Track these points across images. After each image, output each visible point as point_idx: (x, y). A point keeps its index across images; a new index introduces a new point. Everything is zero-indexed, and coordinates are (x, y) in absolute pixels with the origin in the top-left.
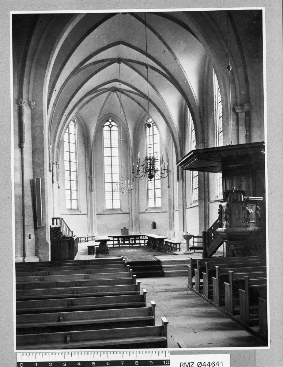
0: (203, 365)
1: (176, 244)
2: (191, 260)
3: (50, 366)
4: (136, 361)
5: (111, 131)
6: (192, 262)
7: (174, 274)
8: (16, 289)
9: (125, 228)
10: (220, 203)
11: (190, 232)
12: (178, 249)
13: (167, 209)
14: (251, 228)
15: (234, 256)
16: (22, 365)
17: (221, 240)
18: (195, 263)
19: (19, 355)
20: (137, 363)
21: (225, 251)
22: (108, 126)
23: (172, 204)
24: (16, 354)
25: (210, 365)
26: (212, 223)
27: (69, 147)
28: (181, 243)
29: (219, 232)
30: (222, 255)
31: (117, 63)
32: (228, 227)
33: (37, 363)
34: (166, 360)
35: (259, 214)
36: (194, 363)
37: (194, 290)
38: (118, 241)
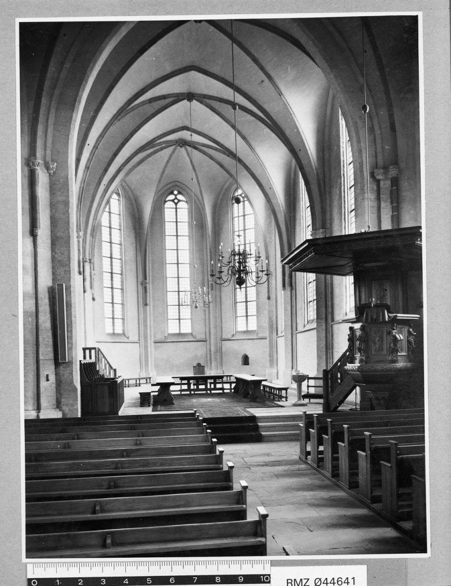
0: (323, 583)
1: (280, 389)
2: (304, 416)
3: (79, 584)
4: (217, 576)
5: (176, 208)
6: (306, 419)
7: (277, 438)
8: (26, 461)
9: (199, 365)
10: (351, 325)
11: (303, 370)
12: (284, 397)
13: (267, 334)
14: (401, 364)
15: (372, 408)
16: (34, 583)
17: (353, 383)
18: (310, 420)
19: (30, 567)
20: (218, 579)
21: (358, 401)
22: (173, 201)
23: (275, 326)
24: (26, 565)
25: (334, 583)
26: (337, 355)
27: (110, 235)
28: (288, 388)
29: (349, 371)
30: (354, 407)
31: (186, 100)
32: (364, 363)
33: (59, 579)
34: (264, 575)
35: (413, 342)
36: (308, 579)
37: (310, 462)
38: (189, 384)
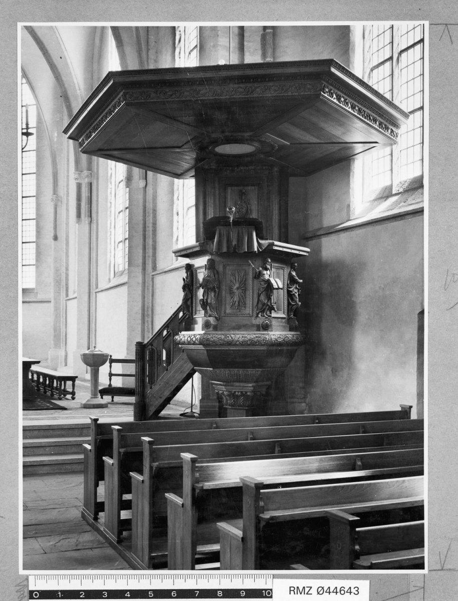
2: (93, 427)
6: (97, 434)
7: (46, 468)
10: (187, 261)
11: (102, 347)
12: (69, 393)
13: (51, 295)
14: (277, 333)
15: (222, 413)
17: (189, 366)
18: (106, 437)
21: (197, 402)
23: (63, 283)
26: (160, 320)
28: (77, 377)
29: (184, 343)
30: (189, 410)
32: (211, 329)
35: (297, 295)
37: (102, 529)
